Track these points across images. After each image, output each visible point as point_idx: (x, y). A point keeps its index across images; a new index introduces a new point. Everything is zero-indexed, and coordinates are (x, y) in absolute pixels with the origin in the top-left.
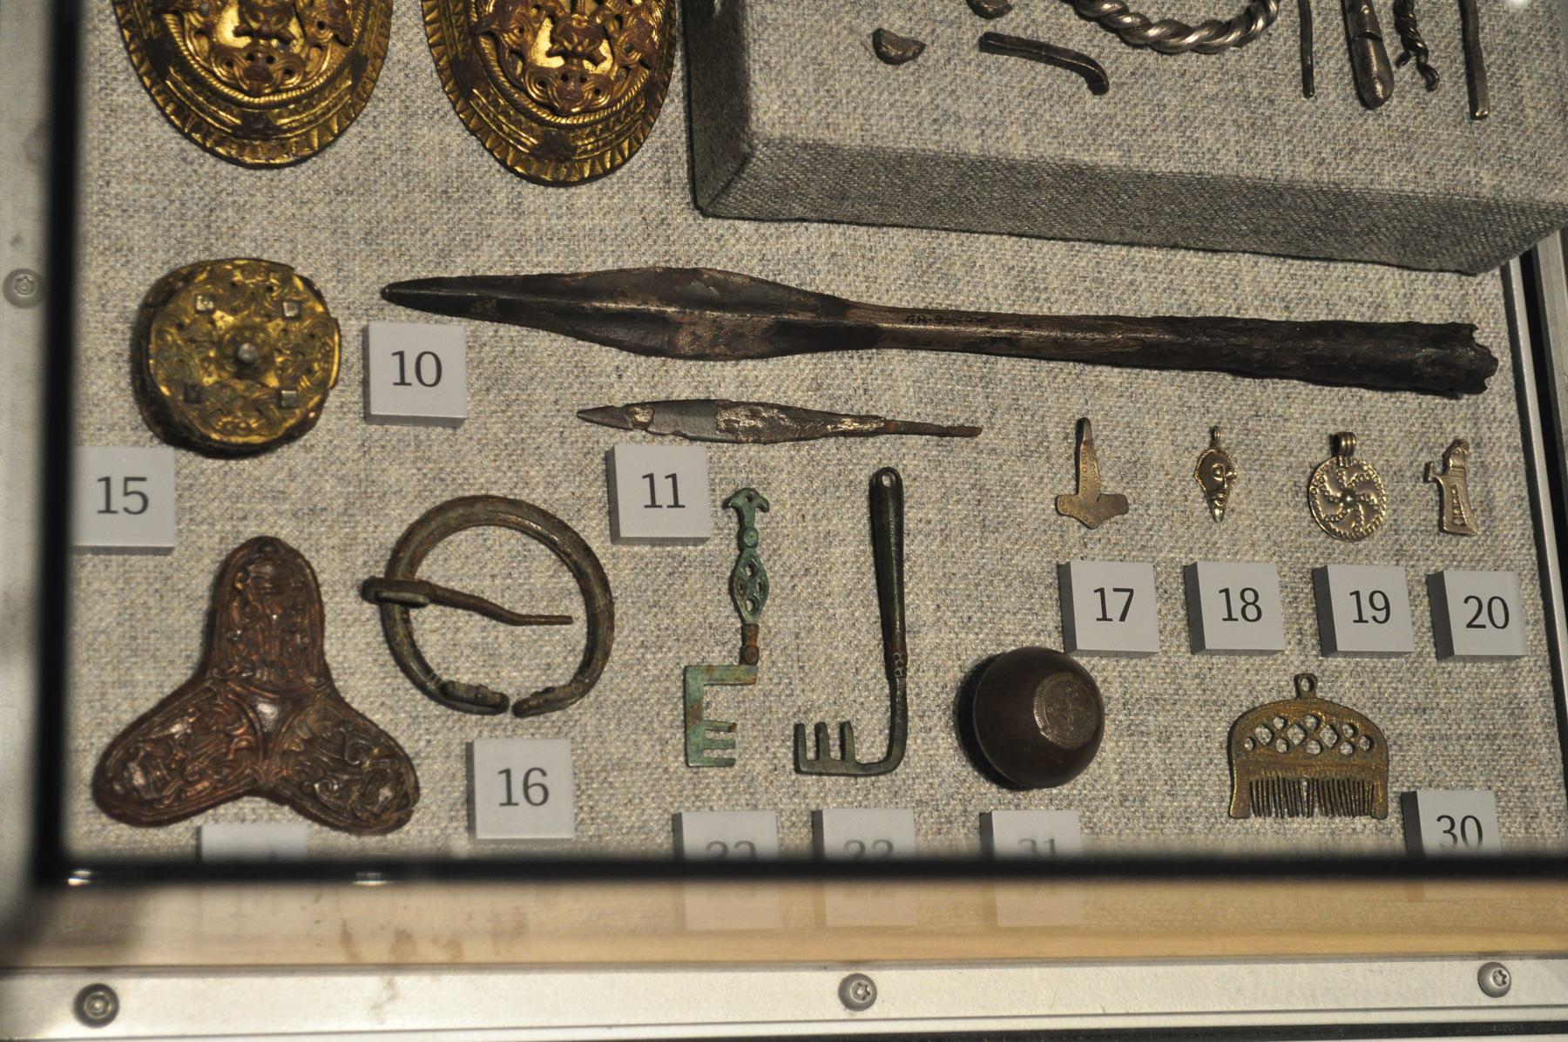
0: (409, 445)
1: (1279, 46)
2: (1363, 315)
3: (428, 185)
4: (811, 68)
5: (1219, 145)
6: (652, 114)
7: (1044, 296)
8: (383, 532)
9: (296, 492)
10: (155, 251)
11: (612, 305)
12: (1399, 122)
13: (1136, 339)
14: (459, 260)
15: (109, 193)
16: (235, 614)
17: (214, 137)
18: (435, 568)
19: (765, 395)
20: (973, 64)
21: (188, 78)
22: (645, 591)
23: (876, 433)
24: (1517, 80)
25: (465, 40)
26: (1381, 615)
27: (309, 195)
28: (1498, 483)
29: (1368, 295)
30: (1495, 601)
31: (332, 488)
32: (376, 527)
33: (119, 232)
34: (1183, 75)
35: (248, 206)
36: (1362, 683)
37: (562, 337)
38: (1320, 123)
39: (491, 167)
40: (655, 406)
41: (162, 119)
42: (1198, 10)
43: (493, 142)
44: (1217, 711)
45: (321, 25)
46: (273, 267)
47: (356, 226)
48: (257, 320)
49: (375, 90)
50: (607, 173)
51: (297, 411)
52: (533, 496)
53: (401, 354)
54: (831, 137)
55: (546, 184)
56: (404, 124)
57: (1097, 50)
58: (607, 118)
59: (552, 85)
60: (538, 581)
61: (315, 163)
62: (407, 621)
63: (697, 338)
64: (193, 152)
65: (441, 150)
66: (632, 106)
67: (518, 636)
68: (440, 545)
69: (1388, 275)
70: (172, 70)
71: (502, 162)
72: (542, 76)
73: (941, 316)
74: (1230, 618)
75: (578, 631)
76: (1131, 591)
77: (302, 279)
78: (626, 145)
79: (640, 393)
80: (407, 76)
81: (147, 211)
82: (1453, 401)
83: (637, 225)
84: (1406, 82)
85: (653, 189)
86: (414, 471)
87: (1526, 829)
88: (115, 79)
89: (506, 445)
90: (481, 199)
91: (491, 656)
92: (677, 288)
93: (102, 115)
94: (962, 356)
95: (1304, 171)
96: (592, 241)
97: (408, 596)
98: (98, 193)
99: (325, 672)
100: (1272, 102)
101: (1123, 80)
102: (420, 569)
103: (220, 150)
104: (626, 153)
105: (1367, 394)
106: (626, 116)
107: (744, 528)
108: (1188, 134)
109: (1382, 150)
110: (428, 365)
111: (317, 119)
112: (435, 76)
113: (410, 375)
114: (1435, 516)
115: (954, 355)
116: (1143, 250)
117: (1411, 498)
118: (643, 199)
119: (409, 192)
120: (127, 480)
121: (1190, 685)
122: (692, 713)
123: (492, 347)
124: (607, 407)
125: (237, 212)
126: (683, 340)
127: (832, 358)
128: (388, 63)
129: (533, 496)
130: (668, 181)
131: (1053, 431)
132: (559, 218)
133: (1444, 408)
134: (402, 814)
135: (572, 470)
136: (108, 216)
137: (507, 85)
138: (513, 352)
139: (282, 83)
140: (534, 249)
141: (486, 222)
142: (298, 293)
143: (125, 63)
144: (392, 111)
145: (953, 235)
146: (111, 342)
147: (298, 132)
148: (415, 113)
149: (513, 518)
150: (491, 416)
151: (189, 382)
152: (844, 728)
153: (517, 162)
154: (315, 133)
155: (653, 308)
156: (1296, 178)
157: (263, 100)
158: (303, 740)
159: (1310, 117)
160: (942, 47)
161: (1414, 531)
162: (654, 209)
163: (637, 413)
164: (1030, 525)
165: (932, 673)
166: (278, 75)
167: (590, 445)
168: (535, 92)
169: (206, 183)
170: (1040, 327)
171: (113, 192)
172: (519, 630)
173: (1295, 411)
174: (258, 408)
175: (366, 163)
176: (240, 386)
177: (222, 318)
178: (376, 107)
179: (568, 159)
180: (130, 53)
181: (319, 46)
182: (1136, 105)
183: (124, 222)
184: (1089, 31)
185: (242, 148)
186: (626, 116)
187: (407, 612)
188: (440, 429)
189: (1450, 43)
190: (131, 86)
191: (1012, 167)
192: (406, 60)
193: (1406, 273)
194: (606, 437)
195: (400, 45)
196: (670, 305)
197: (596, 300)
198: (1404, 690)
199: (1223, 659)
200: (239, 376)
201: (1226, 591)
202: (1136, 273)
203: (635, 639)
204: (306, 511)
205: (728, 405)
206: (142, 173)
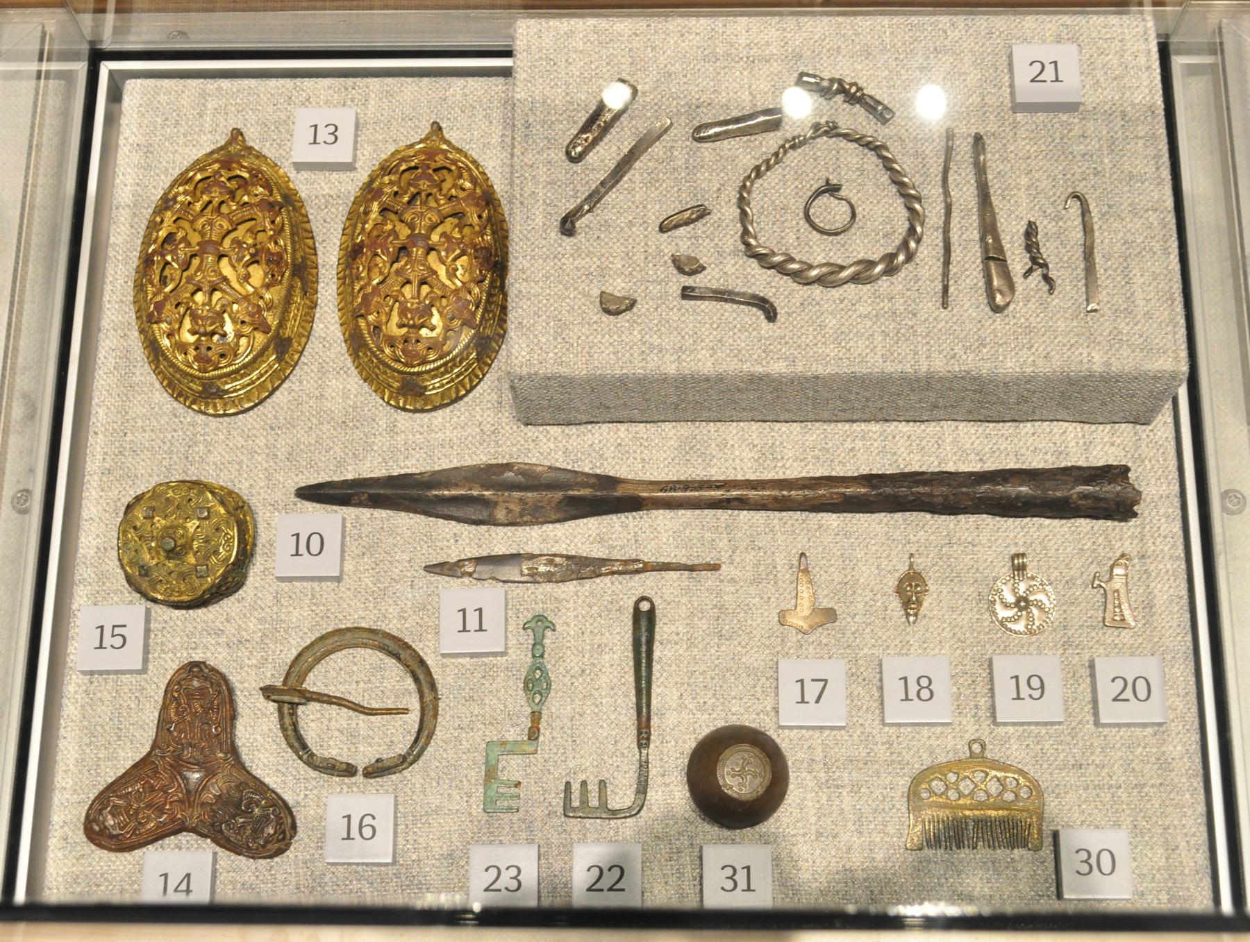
1: (924, 272)
2: (1046, 462)
4: (552, 324)
5: (868, 351)
6: (489, 357)
7: (780, 464)
11: (446, 493)
12: (1023, 320)
13: (837, 493)
14: (350, 468)
18: (313, 682)
19: (562, 548)
20: (675, 310)
23: (637, 572)
24: (1131, 279)
26: (1037, 694)
28: (1159, 586)
29: (1051, 445)
30: (1139, 680)
34: (842, 302)
36: (1028, 745)
38: (955, 327)
40: (479, 560)
42: (859, 253)
44: (901, 769)
49: (302, 358)
51: (209, 579)
52: (391, 626)
53: (297, 535)
54: (564, 371)
55: (448, 405)
57: (774, 290)
58: (445, 364)
63: (509, 511)
64: (180, 408)
69: (1071, 429)
73: (687, 485)
74: (907, 699)
75: (414, 717)
76: (826, 681)
82: (1123, 524)
84: (1032, 289)
85: (489, 409)
87: (1167, 859)
91: (353, 736)
92: (494, 477)
94: (714, 511)
95: (939, 365)
99: (234, 751)
100: (915, 315)
101: (794, 309)
103: (195, 407)
105: (1048, 521)
107: (538, 643)
108: (843, 344)
109: (1006, 343)
111: (253, 383)
112: (343, 344)
113: (303, 549)
114: (1101, 614)
115: (706, 511)
116: (863, 424)
117: (1080, 600)
120: (114, 626)
121: (881, 749)
122: (490, 775)
126: (500, 514)
127: (611, 519)
129: (391, 626)
131: (781, 561)
132: (421, 434)
133: (1114, 530)
134: (281, 844)
139: (219, 363)
142: (208, 501)
143: (143, 356)
145: (712, 424)
151: (141, 563)
152: (602, 784)
153: (390, 399)
155: (475, 493)
156: (932, 370)
158: (214, 795)
159: (947, 322)
160: (652, 299)
161: (1081, 627)
163: (464, 566)
164: (757, 634)
165: (673, 743)
170: (764, 489)
173: (984, 537)
174: (183, 576)
176: (171, 564)
178: (302, 369)
182: (802, 327)
184: (769, 276)
185: (207, 405)
188: (329, 583)
189: (1073, 255)
191: (707, 380)
193: (1087, 426)
195: (321, 326)
196: (487, 490)
197: (436, 490)
198: (1063, 750)
199: (909, 729)
200: (169, 558)
201: (905, 679)
202: (857, 441)
205: (531, 557)
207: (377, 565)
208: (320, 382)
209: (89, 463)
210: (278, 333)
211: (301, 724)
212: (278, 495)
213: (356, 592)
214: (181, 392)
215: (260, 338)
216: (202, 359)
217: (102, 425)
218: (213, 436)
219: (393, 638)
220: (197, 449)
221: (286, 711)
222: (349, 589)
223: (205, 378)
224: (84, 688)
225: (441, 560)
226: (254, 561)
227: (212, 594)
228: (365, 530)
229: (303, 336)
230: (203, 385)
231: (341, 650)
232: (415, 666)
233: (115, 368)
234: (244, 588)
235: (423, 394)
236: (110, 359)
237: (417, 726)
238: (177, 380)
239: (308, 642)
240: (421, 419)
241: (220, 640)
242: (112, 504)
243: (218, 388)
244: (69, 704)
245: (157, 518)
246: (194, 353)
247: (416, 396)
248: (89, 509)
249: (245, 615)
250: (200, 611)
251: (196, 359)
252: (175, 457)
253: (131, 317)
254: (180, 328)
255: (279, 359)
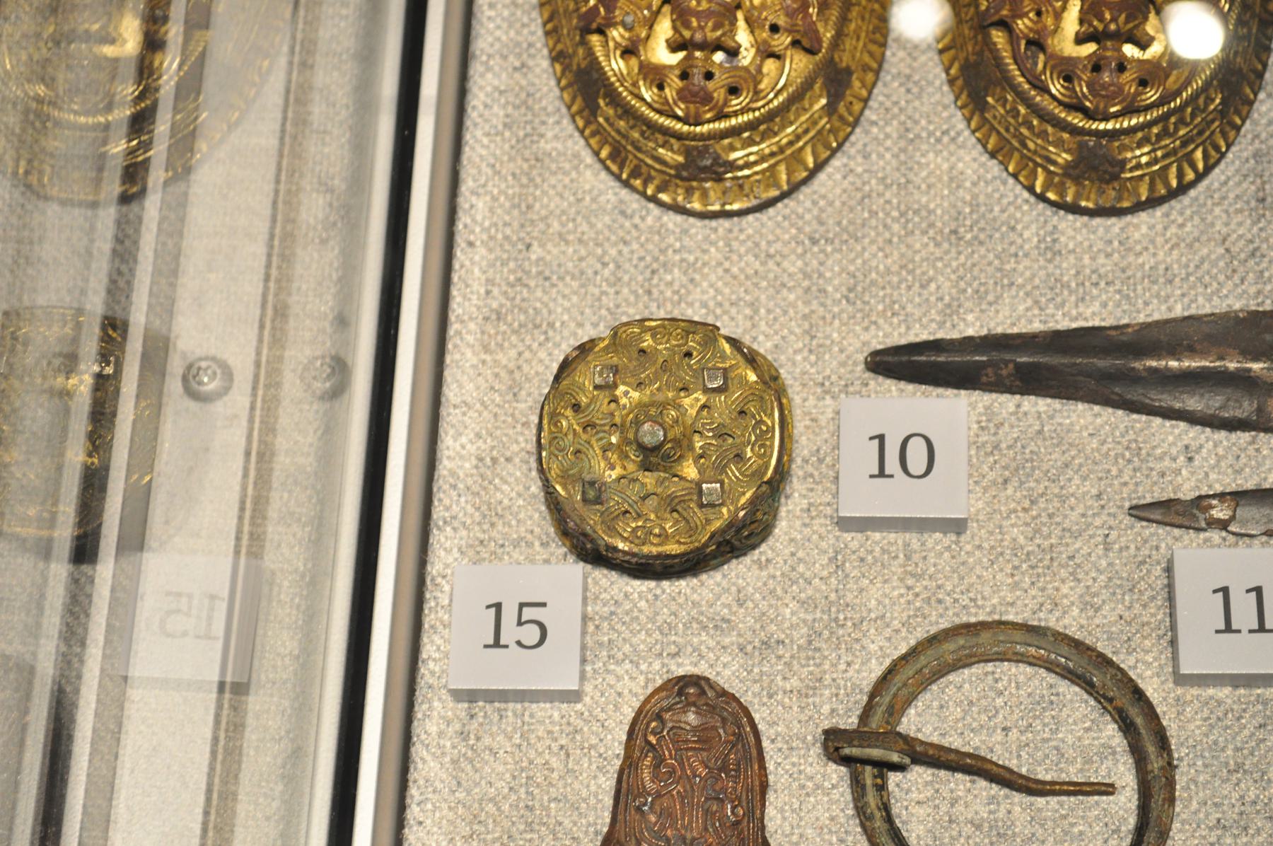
0: (896, 557)
3: (931, 225)
6: (1238, 112)
8: (858, 672)
9: (745, 621)
10: (580, 325)
11: (1173, 364)
14: (970, 317)
15: (529, 259)
16: (646, 775)
17: (656, 182)
21: (620, 111)
22: (1223, 750)
25: (975, 37)
27: (778, 246)
31: (793, 613)
32: (849, 664)
33: (538, 305)
35: (699, 264)
37: (1110, 410)
39: (1016, 197)
40: (1239, 497)
41: (598, 166)
43: (1017, 164)
45: (774, 29)
46: (692, 327)
47: (836, 282)
48: (670, 395)
49: (867, 112)
50: (1173, 194)
51: (724, 510)
52: (1066, 621)
53: (881, 438)
56: (903, 150)
58: (1164, 118)
59: (1080, 79)
60: (1067, 736)
61: (786, 206)
62: (881, 788)
64: (633, 202)
65: (951, 179)
66: (1201, 101)
67: (1040, 810)
68: (934, 687)
70: (601, 102)
71: (1031, 189)
72: (1066, 67)
75: (1125, 803)
77: (730, 340)
78: (1199, 154)
79: (1218, 481)
80: (908, 91)
81: (573, 278)
83: (1218, 259)
85: (1240, 211)
86: (903, 591)
88: (543, 123)
89: (1028, 554)
90: (1002, 238)
93: (525, 166)
96: (1155, 282)
97: (876, 753)
98: (516, 260)
102: (904, 720)
103: (664, 197)
104: (1200, 166)
106: (1193, 116)
110: (917, 453)
111: (782, 150)
112: (946, 88)
113: (892, 464)
118: (1227, 224)
119: (907, 235)
120: (522, 605)
123: (1012, 427)
124: (1170, 501)
125: (685, 273)
128: (885, 77)
129: (1066, 621)
130: (1263, 200)
132: (1108, 256)
135: (1120, 586)
136: (526, 286)
137: (1026, 86)
138: (1040, 432)
139: (726, 103)
140: (1073, 298)
141: (1008, 267)
142: (723, 357)
143: (557, 103)
144: (888, 136)
146: (521, 439)
147: (757, 168)
148: (918, 136)
149: (1032, 650)
150: (1008, 517)
151: (588, 478)
153: (1046, 187)
154: (782, 168)
155: (1232, 366)
157: (705, 128)
162: (1241, 236)
163: (1212, 507)
166: (720, 95)
167: (1147, 552)
168: (1056, 88)
169: (647, 240)
171: (534, 257)
172: (1041, 801)
174: (672, 505)
175: (853, 203)
176: (649, 479)
177: (626, 393)
178: (867, 132)
179: (1116, 177)
180: (562, 89)
181: (778, 57)
183: (544, 291)
185: (689, 192)
186: (1193, 116)
187: (882, 776)
190: (562, 130)
192: (907, 71)
194: (1163, 538)
195: (901, 54)
200: (647, 467)
203: (1207, 815)
204: (757, 644)
206: (569, 232)
207: (1032, 502)
208: (903, 157)
209: (458, 299)
210: (832, 58)
211: (896, 809)
212: (831, 363)
213: (995, 556)
214: (637, 167)
215: (797, 65)
216: (695, 95)
217: (483, 230)
218: (698, 254)
219: (1077, 645)
220: (669, 278)
221: (869, 782)
222: (979, 547)
223: (695, 137)
224: (458, 727)
225: (1168, 494)
226: (788, 490)
227: (719, 545)
228: (1008, 435)
229: (871, 69)
230: (687, 152)
231: (969, 665)
232: (1124, 701)
233: (505, 125)
234: (771, 540)
235: (1116, 177)
236: (496, 108)
237: (1132, 821)
238: (633, 143)
239: (903, 649)
240: (1107, 229)
241: (727, 641)
242: (503, 374)
243: (717, 158)
244: (429, 758)
245: (622, 388)
246: (678, 83)
247: (1102, 180)
248: (461, 387)
249: (772, 592)
250: (683, 583)
251: (682, 95)
252: (625, 291)
253: (533, 33)
254: (648, 37)
255: (830, 109)
